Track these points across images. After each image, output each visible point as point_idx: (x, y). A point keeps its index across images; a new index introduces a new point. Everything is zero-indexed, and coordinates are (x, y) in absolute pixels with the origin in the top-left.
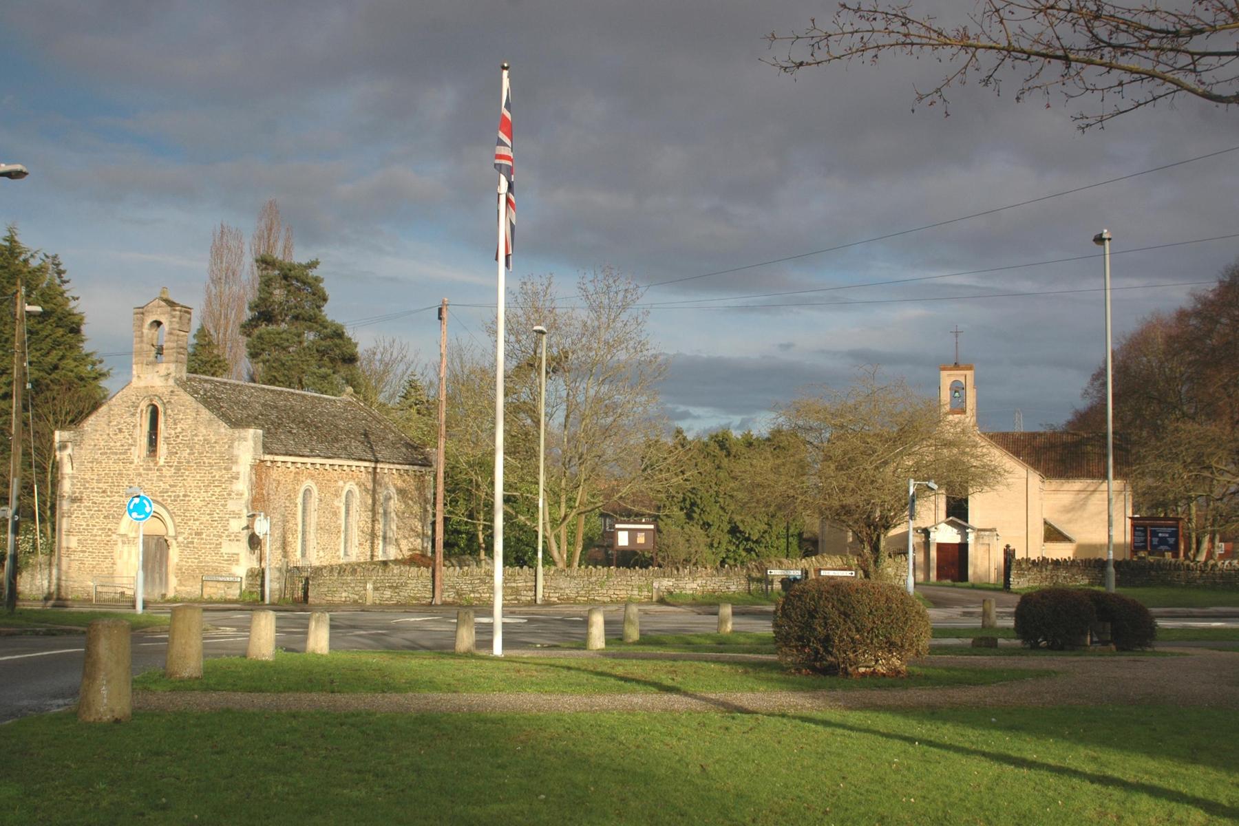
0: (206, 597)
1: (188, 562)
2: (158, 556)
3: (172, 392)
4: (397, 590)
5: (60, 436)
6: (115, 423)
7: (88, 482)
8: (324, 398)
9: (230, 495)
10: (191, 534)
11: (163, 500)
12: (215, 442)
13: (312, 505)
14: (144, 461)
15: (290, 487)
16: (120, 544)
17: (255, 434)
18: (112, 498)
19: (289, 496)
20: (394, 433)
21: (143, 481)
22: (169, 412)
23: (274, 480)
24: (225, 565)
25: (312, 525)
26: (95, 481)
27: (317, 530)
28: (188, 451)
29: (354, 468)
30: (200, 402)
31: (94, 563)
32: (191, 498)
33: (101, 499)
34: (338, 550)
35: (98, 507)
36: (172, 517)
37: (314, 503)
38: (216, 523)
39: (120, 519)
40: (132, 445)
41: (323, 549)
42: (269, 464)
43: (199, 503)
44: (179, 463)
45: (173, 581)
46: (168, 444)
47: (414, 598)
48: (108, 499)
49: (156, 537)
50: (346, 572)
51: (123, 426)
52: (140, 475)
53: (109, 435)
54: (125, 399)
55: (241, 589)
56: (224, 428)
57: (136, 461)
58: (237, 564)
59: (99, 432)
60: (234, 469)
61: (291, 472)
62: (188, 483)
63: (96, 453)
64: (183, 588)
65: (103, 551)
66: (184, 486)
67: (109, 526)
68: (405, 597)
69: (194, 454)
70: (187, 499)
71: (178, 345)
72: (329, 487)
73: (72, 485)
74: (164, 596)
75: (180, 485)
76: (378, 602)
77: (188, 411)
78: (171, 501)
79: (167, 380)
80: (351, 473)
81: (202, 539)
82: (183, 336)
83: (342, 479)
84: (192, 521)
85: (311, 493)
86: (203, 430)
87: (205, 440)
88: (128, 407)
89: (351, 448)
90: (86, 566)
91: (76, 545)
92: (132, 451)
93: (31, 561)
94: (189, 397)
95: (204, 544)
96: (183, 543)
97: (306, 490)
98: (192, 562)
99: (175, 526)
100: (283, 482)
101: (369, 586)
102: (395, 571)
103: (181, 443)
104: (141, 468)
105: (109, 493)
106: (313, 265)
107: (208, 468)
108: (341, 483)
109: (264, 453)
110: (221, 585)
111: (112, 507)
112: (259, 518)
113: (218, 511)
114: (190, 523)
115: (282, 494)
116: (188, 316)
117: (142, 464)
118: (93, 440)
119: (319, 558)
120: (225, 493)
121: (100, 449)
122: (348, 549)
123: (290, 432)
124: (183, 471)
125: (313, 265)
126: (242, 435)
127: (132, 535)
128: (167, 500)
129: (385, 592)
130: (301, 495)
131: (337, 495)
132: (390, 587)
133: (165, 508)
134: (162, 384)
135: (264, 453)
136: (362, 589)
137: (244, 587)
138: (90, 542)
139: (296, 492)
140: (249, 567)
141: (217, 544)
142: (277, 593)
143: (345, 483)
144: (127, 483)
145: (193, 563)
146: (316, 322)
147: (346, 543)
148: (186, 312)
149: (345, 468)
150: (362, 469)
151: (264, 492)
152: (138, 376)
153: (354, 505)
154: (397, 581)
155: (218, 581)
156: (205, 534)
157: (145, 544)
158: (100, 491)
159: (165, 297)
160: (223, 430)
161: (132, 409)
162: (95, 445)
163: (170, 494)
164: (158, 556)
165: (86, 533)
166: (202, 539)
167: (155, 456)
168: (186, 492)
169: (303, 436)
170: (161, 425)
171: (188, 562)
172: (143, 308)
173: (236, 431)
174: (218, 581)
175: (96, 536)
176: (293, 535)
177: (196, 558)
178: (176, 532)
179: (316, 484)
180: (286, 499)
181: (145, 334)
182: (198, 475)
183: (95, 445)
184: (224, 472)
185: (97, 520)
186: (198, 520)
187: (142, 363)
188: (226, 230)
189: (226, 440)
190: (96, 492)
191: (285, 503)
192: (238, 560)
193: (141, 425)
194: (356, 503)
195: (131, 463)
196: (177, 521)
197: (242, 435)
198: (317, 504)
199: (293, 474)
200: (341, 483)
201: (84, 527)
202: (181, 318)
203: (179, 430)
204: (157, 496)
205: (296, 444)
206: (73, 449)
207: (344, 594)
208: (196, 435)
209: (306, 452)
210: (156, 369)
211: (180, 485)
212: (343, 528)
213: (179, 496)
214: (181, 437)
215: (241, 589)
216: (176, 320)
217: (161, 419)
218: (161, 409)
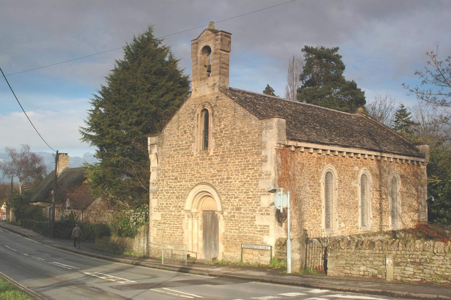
0: (244, 262)
1: (231, 232)
2: (213, 227)
3: (217, 97)
4: (421, 267)
5: (151, 141)
6: (182, 127)
7: (167, 172)
8: (342, 113)
9: (260, 175)
10: (233, 209)
11: (214, 183)
12: (248, 133)
13: (334, 186)
14: (200, 153)
15: (314, 169)
16: (186, 217)
17: (278, 122)
18: (181, 183)
19: (313, 177)
20: (395, 135)
21: (200, 169)
22: (216, 113)
23: (299, 163)
24: (258, 235)
25: (334, 201)
26: (170, 171)
27: (338, 205)
28: (229, 142)
29: (366, 156)
30: (236, 102)
31: (171, 232)
32: (232, 180)
33: (174, 184)
34: (357, 222)
35: (173, 190)
36: (219, 196)
37: (335, 183)
38: (250, 200)
39: (186, 199)
40: (192, 142)
41: (344, 221)
42: (293, 149)
43: (238, 183)
44: (223, 152)
45: (221, 247)
46: (216, 138)
47: (442, 277)
48: (179, 184)
49: (211, 212)
50: (364, 245)
51: (186, 129)
52: (198, 164)
53: (178, 136)
54: (188, 108)
55: (271, 256)
56: (254, 121)
57: (195, 154)
58: (268, 235)
59: (173, 135)
60: (263, 153)
61: (314, 157)
62: (230, 168)
63: (171, 151)
64: (228, 253)
65: (176, 223)
66: (227, 170)
67: (179, 205)
68: (431, 276)
69: (233, 144)
70: (229, 180)
71: (220, 61)
72: (347, 171)
73: (158, 175)
74: (214, 259)
75: (224, 169)
76: (399, 278)
77: (228, 110)
78: (219, 183)
79: (214, 89)
80: (364, 160)
81: (241, 213)
82: (224, 55)
83: (357, 164)
84: (233, 199)
85: (332, 176)
86: (239, 124)
87: (241, 132)
88: (190, 114)
89: (363, 142)
90: (166, 234)
91: (161, 218)
92: (192, 146)
93: (138, 229)
94: (229, 100)
95: (243, 217)
96: (227, 216)
97: (327, 173)
98: (234, 232)
99: (222, 203)
100: (307, 165)
101: (389, 261)
102: (417, 246)
103: (224, 137)
104: (199, 159)
105: (179, 180)
106: (336, 49)
107: (244, 155)
108: (356, 168)
109: (288, 139)
110: (255, 252)
111: (181, 190)
112: (279, 193)
113: (252, 190)
114: (232, 200)
115: (306, 175)
116: (228, 39)
117: (199, 155)
118: (169, 141)
119: (341, 228)
120: (257, 174)
121: (173, 147)
122: (365, 221)
123: (314, 128)
124: (226, 158)
125: (336, 49)
126: (268, 124)
127: (194, 210)
128: (215, 182)
129: (407, 268)
130: (323, 176)
131: (354, 177)
132: (412, 263)
133: (215, 189)
134: (210, 93)
135: (288, 139)
136: (381, 263)
137: (273, 255)
138: (168, 216)
139: (319, 174)
140: (278, 237)
141: (252, 218)
142: (298, 263)
143: (360, 168)
144: (190, 171)
145: (235, 233)
146: (339, 81)
147: (363, 215)
148: (226, 36)
149: (359, 156)
150: (373, 157)
151: (290, 173)
152: (196, 90)
153: (368, 186)
154: (420, 257)
155: (254, 249)
156: (243, 209)
157: (204, 217)
158: (174, 178)
159: (211, 28)
160: (254, 122)
161: (192, 115)
162: (170, 145)
163: (217, 177)
164: (213, 227)
165: (166, 210)
166: (241, 213)
167: (207, 149)
168: (228, 175)
169: (325, 131)
170: (211, 125)
171: (231, 232)
172: (197, 39)
173: (264, 122)
174: (254, 249)
175: (172, 211)
176: (317, 209)
177: (237, 229)
178: (222, 208)
179: (336, 168)
180: (311, 180)
181: (199, 57)
182: (237, 161)
183: (170, 145)
184: (255, 156)
185: (172, 200)
186: (237, 197)
187: (197, 80)
188: (295, 59)
189: (256, 130)
190: (171, 179)
191: (309, 183)
192: (268, 232)
193: (197, 126)
194: (369, 188)
195: (192, 155)
196: (223, 199)
197: (268, 124)
198: (337, 184)
199: (315, 158)
200: (356, 168)
201: (165, 205)
202: (222, 40)
203: (223, 126)
204: (208, 180)
205: (318, 135)
206: (158, 149)
207: (362, 268)
208: (235, 129)
209: (327, 141)
210: (206, 82)
211: (224, 169)
212: (360, 204)
213: (224, 179)
214: (224, 132)
215: (271, 256)
216: (219, 42)
217: (211, 119)
218: (210, 112)
